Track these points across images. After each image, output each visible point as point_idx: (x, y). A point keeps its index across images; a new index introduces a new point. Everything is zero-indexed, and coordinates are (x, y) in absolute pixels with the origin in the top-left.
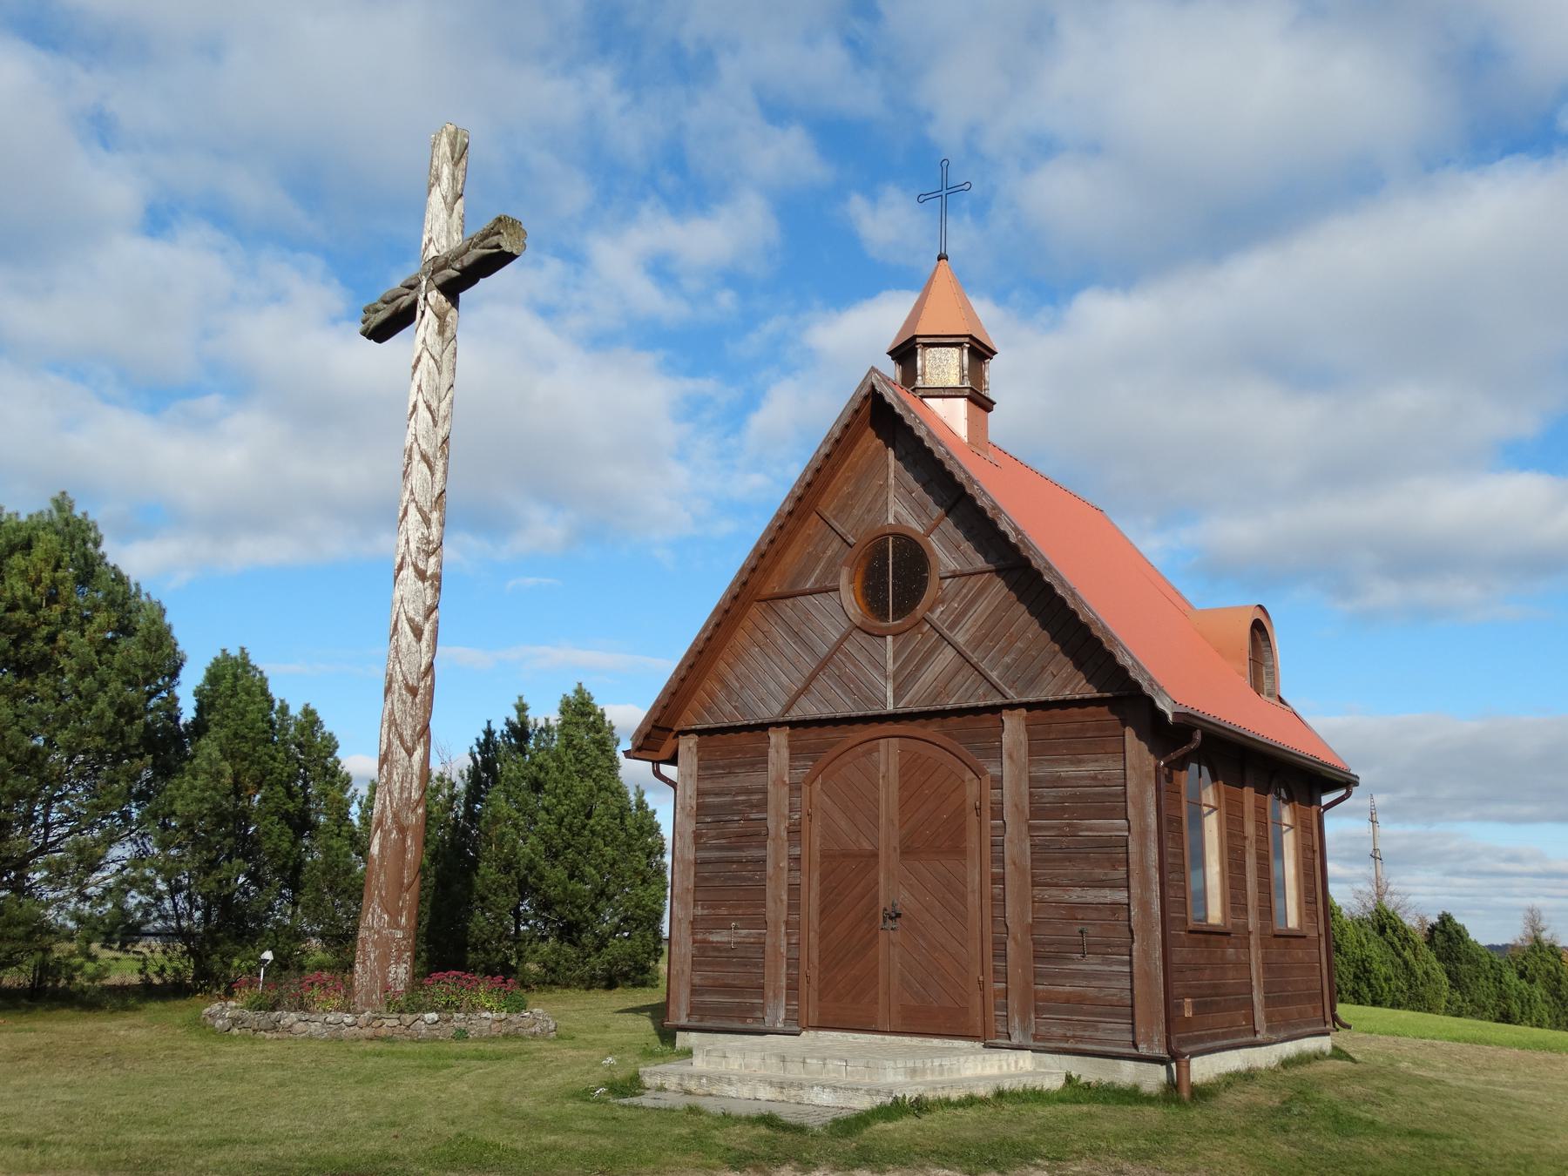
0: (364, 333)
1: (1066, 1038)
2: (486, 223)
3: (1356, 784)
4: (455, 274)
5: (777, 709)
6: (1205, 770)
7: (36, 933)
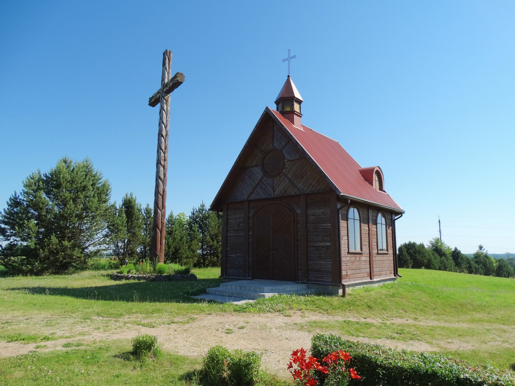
0: (149, 105)
1: (315, 281)
2: (176, 73)
3: (404, 213)
4: (168, 88)
5: (246, 198)
6: (355, 210)
7: (410, 252)
